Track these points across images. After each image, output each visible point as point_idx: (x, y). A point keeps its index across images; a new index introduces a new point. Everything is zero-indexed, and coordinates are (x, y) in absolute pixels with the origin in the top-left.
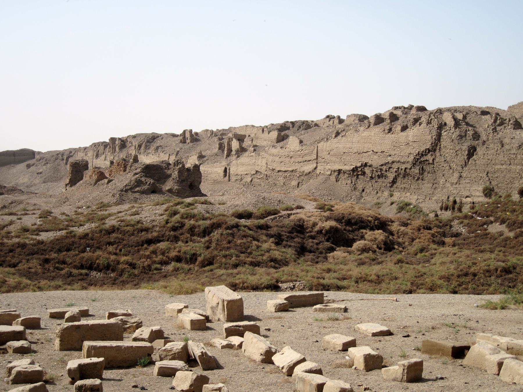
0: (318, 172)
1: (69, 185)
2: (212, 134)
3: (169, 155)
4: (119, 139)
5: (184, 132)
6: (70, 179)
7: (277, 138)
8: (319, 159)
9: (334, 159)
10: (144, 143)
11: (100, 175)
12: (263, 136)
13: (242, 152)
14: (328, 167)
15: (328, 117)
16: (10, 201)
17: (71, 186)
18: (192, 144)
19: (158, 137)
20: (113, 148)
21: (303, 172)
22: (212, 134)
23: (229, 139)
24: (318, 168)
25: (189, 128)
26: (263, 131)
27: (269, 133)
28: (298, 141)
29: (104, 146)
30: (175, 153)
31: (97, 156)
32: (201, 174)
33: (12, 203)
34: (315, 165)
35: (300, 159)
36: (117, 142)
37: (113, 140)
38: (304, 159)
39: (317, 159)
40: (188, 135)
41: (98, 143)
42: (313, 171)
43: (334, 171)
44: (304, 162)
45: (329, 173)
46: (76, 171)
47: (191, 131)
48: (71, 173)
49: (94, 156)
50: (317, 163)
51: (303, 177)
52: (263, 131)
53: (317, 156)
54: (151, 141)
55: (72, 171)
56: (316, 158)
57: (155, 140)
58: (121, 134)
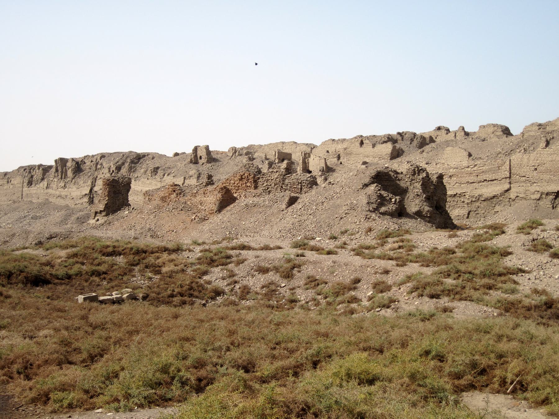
0: (512, 195)
1: (104, 214)
2: (235, 152)
3: (185, 178)
4: (73, 160)
5: (196, 149)
6: (106, 204)
7: (392, 153)
8: (513, 177)
9: (546, 177)
10: (127, 165)
11: (226, 193)
12: (361, 150)
13: (328, 172)
14: (534, 188)
15: (439, 128)
16: (47, 235)
17: (107, 215)
18: (210, 165)
19: (144, 156)
20: (62, 172)
21: (480, 196)
22: (235, 152)
23: (305, 154)
24: (512, 190)
25: (202, 143)
26: (362, 143)
27: (374, 146)
28: (466, 154)
29: (43, 169)
30: (196, 176)
31: (30, 183)
32: (446, 189)
33: (51, 237)
34: (507, 186)
35: (472, 179)
36: (69, 164)
37: (62, 162)
38: (481, 178)
39: (510, 177)
40: (202, 153)
41: (29, 166)
42: (502, 195)
43: (547, 194)
44: (479, 182)
45: (537, 196)
46: (115, 193)
47: (207, 148)
48: (108, 196)
49: (25, 184)
50: (510, 183)
51: (478, 204)
52: (362, 143)
53: (510, 173)
54: (136, 161)
55: (109, 192)
56: (508, 175)
57: (141, 160)
58: (74, 152)
